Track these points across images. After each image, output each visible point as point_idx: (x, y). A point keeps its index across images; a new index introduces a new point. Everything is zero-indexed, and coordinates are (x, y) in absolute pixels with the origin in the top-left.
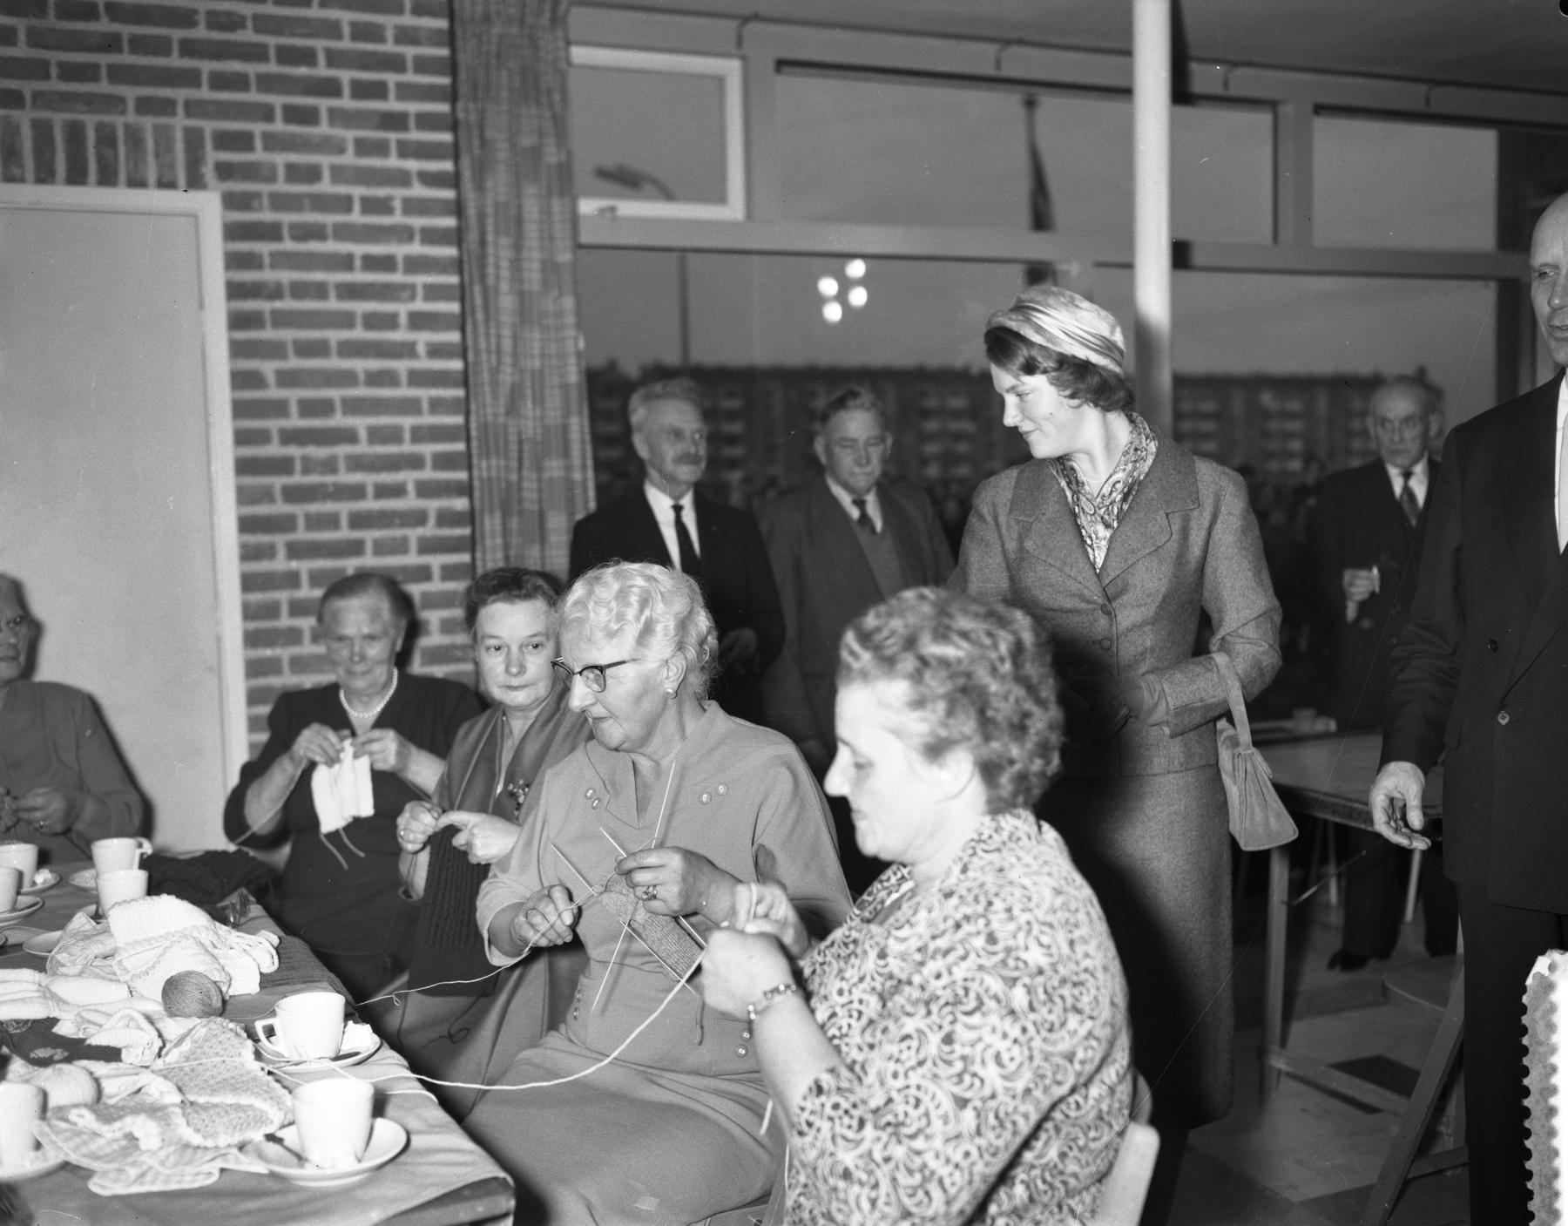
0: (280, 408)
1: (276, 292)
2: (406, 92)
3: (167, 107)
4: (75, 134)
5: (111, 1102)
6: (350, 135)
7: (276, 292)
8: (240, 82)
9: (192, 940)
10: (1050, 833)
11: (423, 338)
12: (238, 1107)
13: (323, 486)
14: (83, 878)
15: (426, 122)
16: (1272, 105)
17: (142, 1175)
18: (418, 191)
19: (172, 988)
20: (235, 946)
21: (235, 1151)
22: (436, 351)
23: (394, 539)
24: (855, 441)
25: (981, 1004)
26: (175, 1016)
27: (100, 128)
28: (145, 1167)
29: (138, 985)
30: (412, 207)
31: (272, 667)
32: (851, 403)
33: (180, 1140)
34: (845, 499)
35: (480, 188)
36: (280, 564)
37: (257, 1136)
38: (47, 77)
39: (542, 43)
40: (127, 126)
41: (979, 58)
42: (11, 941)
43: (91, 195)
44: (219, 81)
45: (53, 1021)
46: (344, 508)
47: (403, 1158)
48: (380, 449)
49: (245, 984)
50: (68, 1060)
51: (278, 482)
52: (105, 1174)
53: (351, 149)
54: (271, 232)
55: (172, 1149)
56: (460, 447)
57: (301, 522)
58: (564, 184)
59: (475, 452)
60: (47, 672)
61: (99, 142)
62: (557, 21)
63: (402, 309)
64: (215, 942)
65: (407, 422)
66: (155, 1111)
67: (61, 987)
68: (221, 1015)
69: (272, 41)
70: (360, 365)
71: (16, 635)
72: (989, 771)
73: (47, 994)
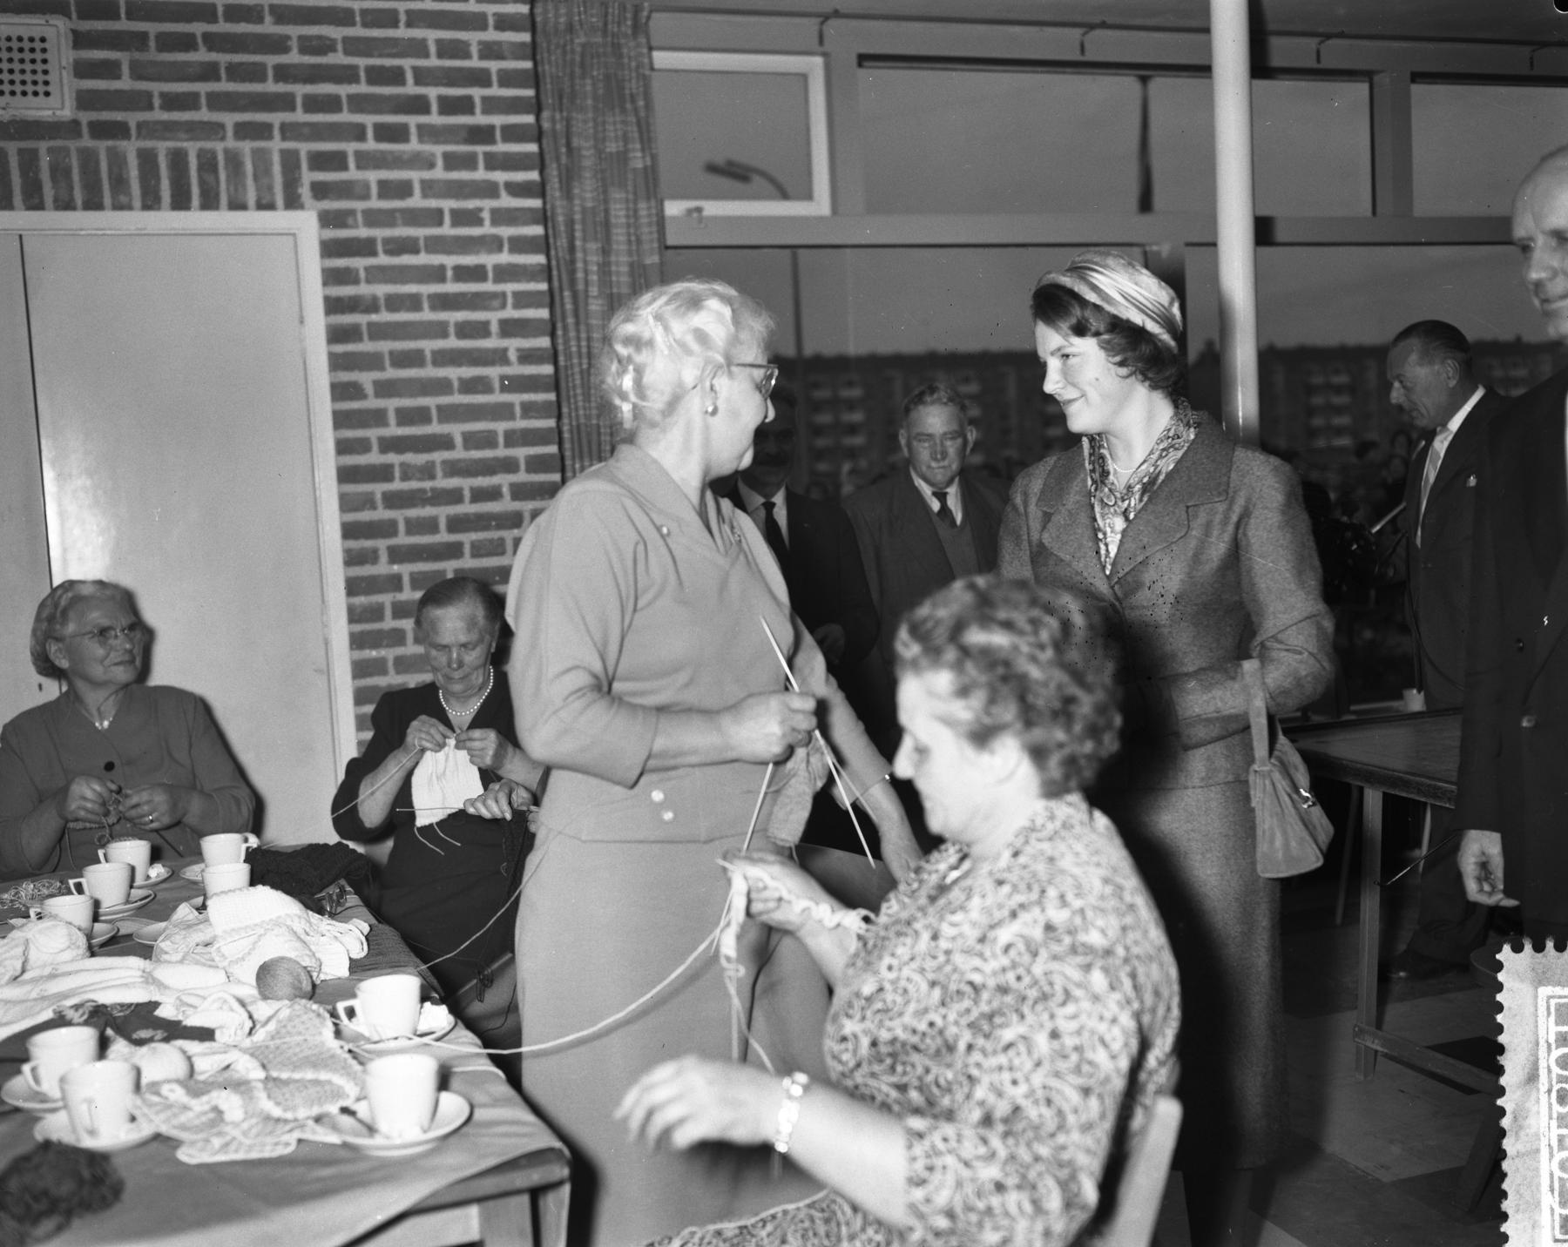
0: (378, 418)
1: (372, 306)
2: (491, 105)
3: (263, 131)
4: (178, 161)
5: (201, 1078)
6: (438, 150)
7: (372, 306)
8: (332, 104)
9: (284, 928)
10: (1102, 820)
11: (513, 345)
12: (316, 1082)
13: (423, 491)
14: (192, 872)
15: (512, 134)
16: (1367, 75)
17: (227, 1145)
18: (507, 201)
19: (265, 973)
20: (327, 934)
21: (311, 1123)
22: (527, 357)
23: (491, 541)
24: (930, 436)
25: (1067, 993)
26: (269, 998)
27: (201, 154)
28: (228, 1138)
29: (236, 971)
30: (500, 217)
31: (378, 667)
32: (928, 399)
33: (262, 1111)
34: (926, 490)
35: (568, 195)
36: (383, 568)
37: (333, 1109)
38: (150, 107)
39: (625, 51)
40: (226, 151)
41: (1061, 44)
42: (123, 932)
43: (197, 219)
44: (313, 104)
45: (155, 1005)
46: (443, 513)
47: (465, 1129)
48: (476, 454)
49: (335, 968)
50: (166, 1040)
51: (378, 489)
52: (193, 1143)
53: (440, 162)
54: (365, 248)
55: (254, 1121)
56: (553, 449)
57: (402, 527)
58: (651, 187)
59: (568, 454)
60: (161, 675)
61: (200, 168)
62: (639, 28)
63: (493, 317)
64: (308, 930)
65: (501, 427)
66: (240, 1086)
67: (162, 973)
68: (310, 999)
69: (362, 62)
70: (454, 373)
71: (131, 640)
72: (1038, 754)
73: (149, 979)
